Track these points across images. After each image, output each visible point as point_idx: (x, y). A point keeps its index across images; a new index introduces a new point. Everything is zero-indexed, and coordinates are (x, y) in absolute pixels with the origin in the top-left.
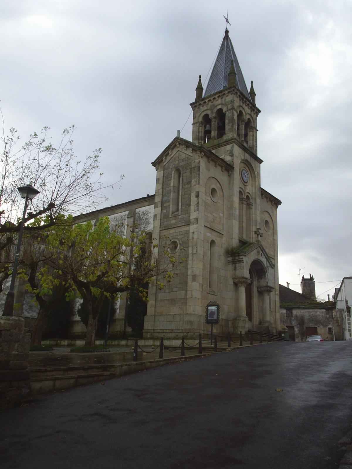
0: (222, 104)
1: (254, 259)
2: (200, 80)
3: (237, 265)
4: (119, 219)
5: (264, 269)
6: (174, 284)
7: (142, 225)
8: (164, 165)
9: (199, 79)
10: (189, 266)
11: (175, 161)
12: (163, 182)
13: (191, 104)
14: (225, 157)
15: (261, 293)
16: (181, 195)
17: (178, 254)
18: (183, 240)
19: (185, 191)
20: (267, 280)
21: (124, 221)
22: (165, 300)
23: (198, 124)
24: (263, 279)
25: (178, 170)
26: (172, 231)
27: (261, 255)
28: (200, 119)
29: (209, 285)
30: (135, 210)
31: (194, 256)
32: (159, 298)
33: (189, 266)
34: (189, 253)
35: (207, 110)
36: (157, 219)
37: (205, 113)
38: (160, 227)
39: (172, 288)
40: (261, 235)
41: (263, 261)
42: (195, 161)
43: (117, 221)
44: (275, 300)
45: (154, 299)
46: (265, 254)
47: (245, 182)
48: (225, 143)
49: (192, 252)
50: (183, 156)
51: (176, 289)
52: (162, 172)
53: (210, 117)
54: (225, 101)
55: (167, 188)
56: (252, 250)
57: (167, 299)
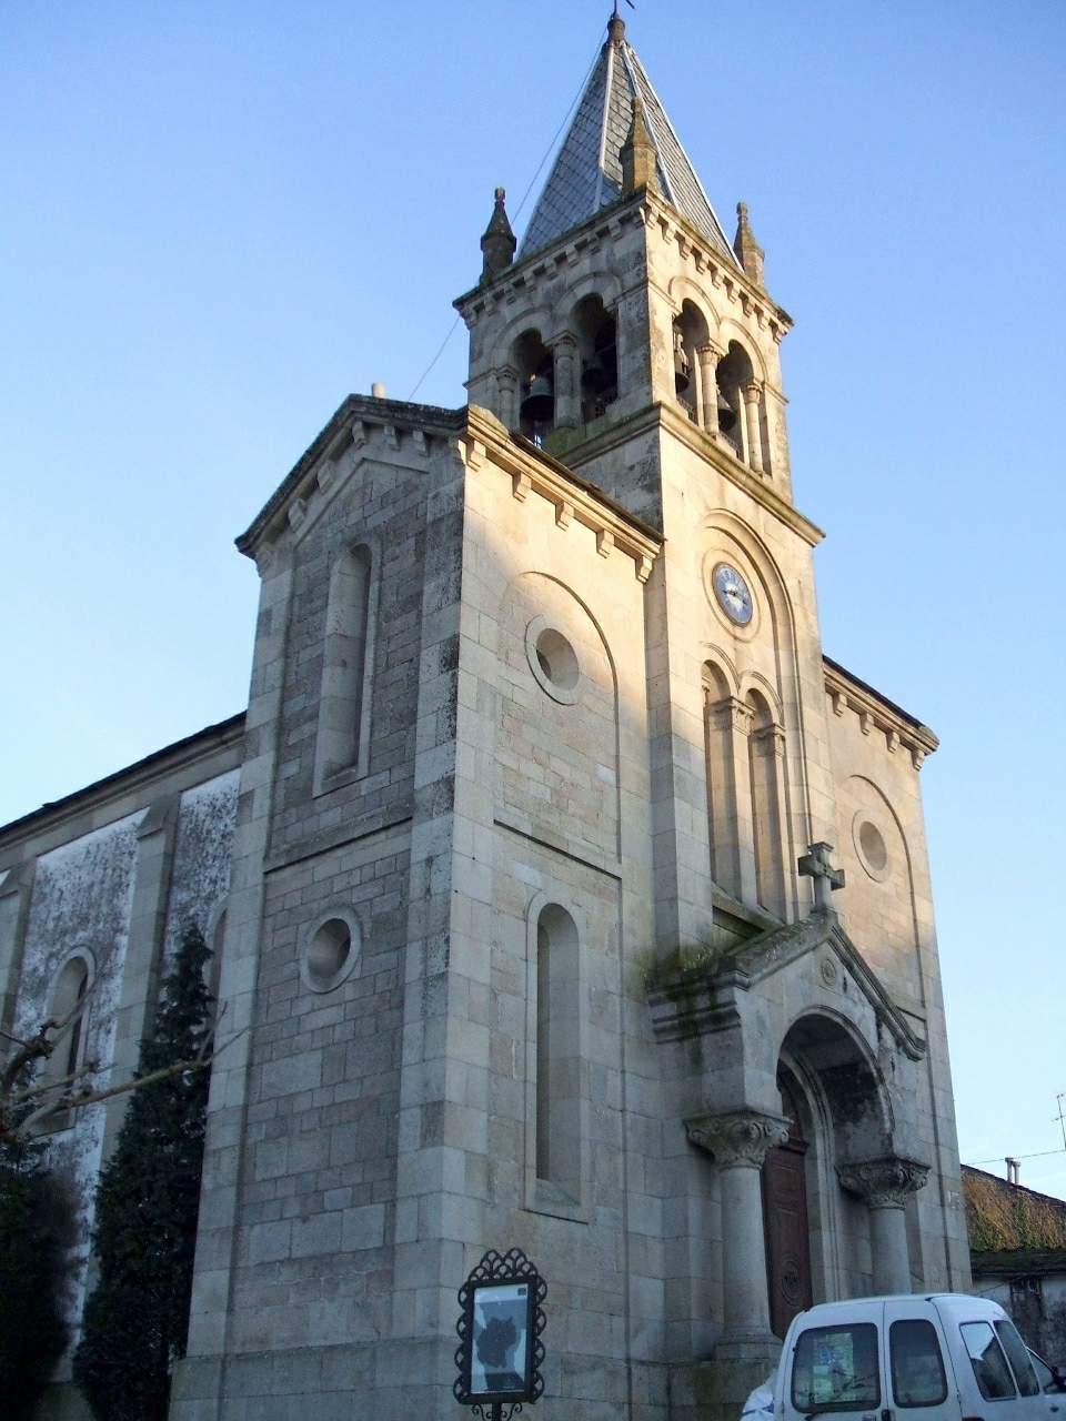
0: (595, 274)
1: (802, 1005)
2: (499, 206)
3: (708, 1042)
4: (105, 852)
5: (866, 1062)
6: (329, 1168)
7: (206, 868)
8: (295, 543)
9: (496, 204)
10: (406, 1052)
11: (347, 514)
12: (287, 634)
15: (855, 1198)
16: (371, 674)
17: (349, 992)
18: (377, 910)
19: (392, 647)
20: (888, 1125)
21: (126, 858)
22: (282, 1262)
23: (492, 380)
24: (865, 1120)
25: (360, 553)
26: (323, 868)
27: (845, 988)
28: (503, 356)
29: (532, 1159)
30: (180, 797)
31: (432, 992)
32: (253, 1256)
33: (409, 1056)
34: (408, 979)
35: (527, 313)
36: (255, 815)
37: (522, 327)
38: (266, 857)
39: (320, 1187)
40: (837, 878)
41: (856, 1021)
42: (441, 489)
43: (96, 865)
44: (946, 1238)
45: (227, 1261)
46: (868, 986)
48: (615, 435)
49: (425, 971)
50: (385, 479)
51: (339, 1192)
52: (287, 576)
53: (545, 338)
54: (608, 261)
55: (308, 651)
56: (789, 957)
57: (289, 1259)
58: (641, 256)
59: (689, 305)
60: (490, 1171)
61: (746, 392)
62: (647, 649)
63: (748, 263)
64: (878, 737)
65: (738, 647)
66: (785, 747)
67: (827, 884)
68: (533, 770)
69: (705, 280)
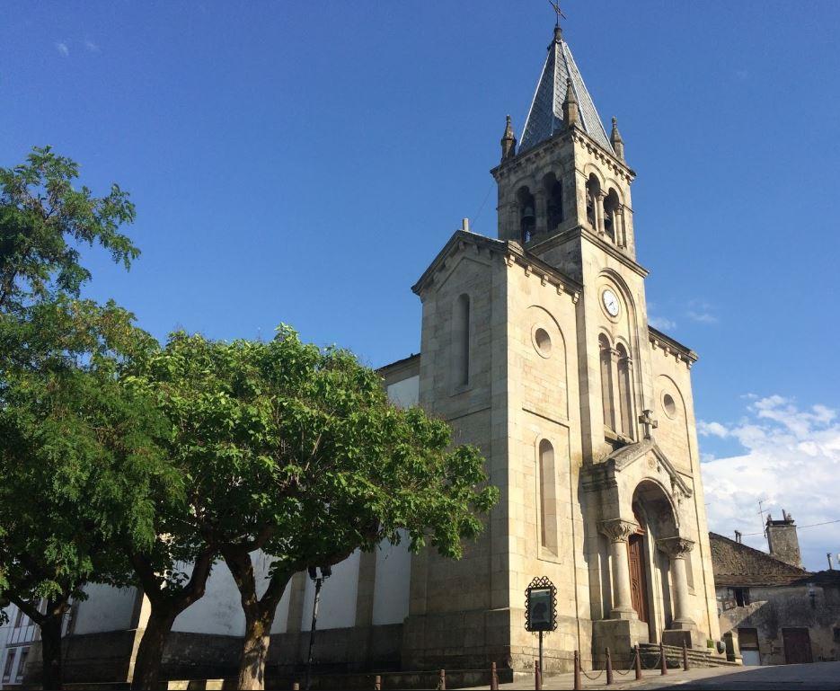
13: (493, 172)
14: (564, 265)
28: (513, 197)
47: (611, 316)
58: (572, 156)
59: (592, 175)
60: (525, 542)
61: (616, 211)
62: (577, 332)
63: (617, 147)
64: (672, 358)
65: (611, 432)
66: (632, 367)
67: (650, 426)
68: (535, 386)
69: (599, 163)
